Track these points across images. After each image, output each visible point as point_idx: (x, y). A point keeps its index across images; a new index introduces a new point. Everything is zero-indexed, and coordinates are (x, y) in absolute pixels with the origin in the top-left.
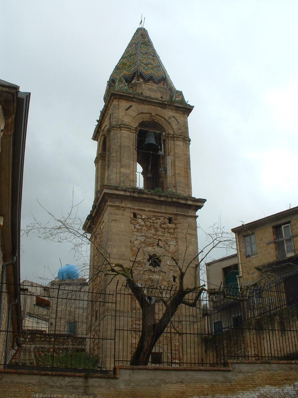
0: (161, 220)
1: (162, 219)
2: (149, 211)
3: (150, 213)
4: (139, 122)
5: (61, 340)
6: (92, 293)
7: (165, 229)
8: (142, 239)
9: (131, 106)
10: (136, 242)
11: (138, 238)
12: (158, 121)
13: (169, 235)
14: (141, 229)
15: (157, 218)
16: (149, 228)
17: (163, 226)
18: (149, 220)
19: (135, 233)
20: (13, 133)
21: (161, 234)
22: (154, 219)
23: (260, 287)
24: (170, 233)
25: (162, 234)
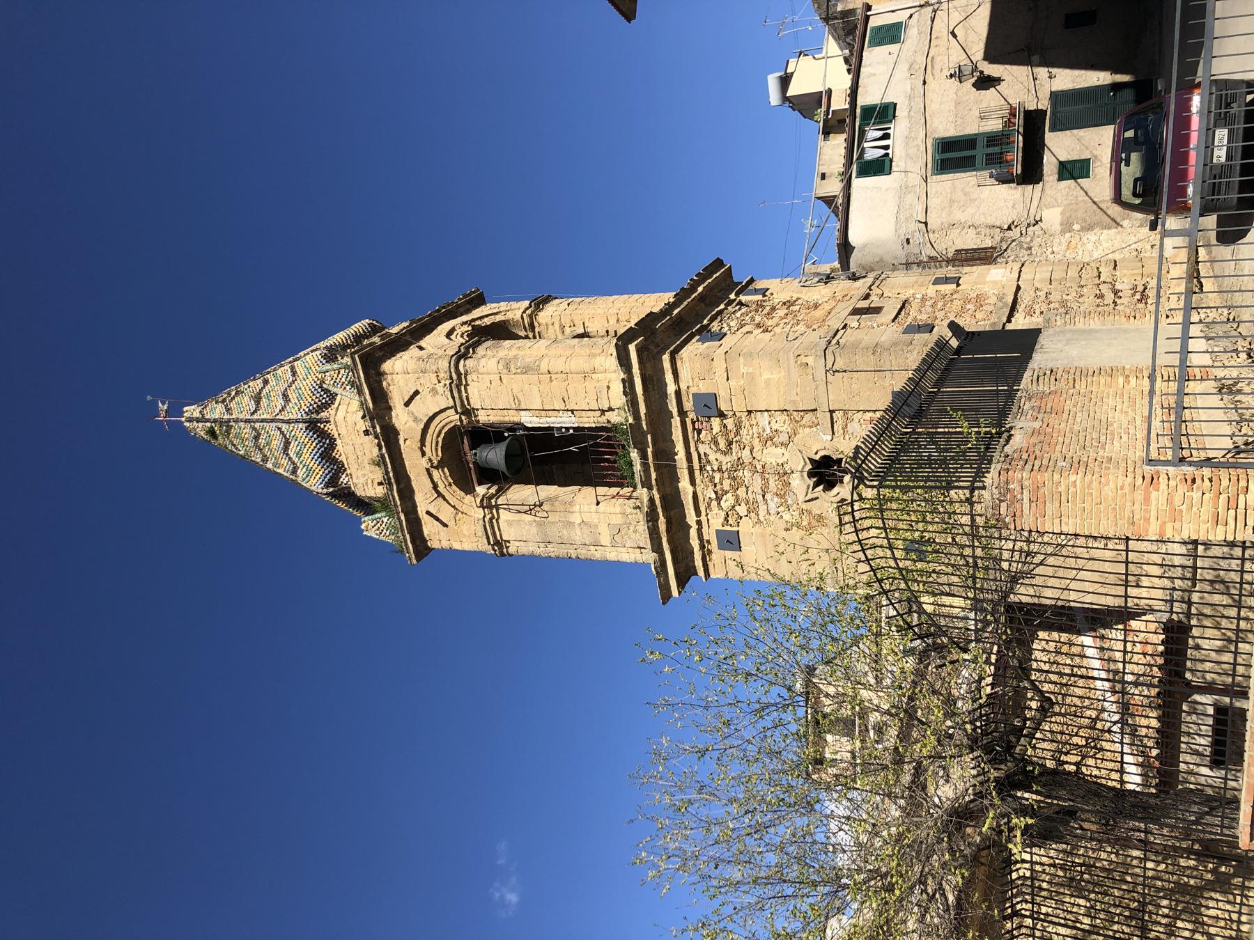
0: (709, 451)
1: (703, 448)
2: (693, 482)
3: (698, 481)
4: (463, 494)
5: (978, 724)
6: (1127, 563)
7: (730, 443)
8: (773, 502)
9: (428, 513)
10: (787, 516)
11: (772, 512)
12: (440, 432)
13: (744, 432)
14: (747, 502)
15: (704, 462)
16: (737, 483)
17: (722, 445)
18: (717, 480)
19: (762, 519)
20: (1214, 682)
21: (747, 452)
22: (708, 468)
23: (965, 181)
24: (739, 425)
25: (747, 448)
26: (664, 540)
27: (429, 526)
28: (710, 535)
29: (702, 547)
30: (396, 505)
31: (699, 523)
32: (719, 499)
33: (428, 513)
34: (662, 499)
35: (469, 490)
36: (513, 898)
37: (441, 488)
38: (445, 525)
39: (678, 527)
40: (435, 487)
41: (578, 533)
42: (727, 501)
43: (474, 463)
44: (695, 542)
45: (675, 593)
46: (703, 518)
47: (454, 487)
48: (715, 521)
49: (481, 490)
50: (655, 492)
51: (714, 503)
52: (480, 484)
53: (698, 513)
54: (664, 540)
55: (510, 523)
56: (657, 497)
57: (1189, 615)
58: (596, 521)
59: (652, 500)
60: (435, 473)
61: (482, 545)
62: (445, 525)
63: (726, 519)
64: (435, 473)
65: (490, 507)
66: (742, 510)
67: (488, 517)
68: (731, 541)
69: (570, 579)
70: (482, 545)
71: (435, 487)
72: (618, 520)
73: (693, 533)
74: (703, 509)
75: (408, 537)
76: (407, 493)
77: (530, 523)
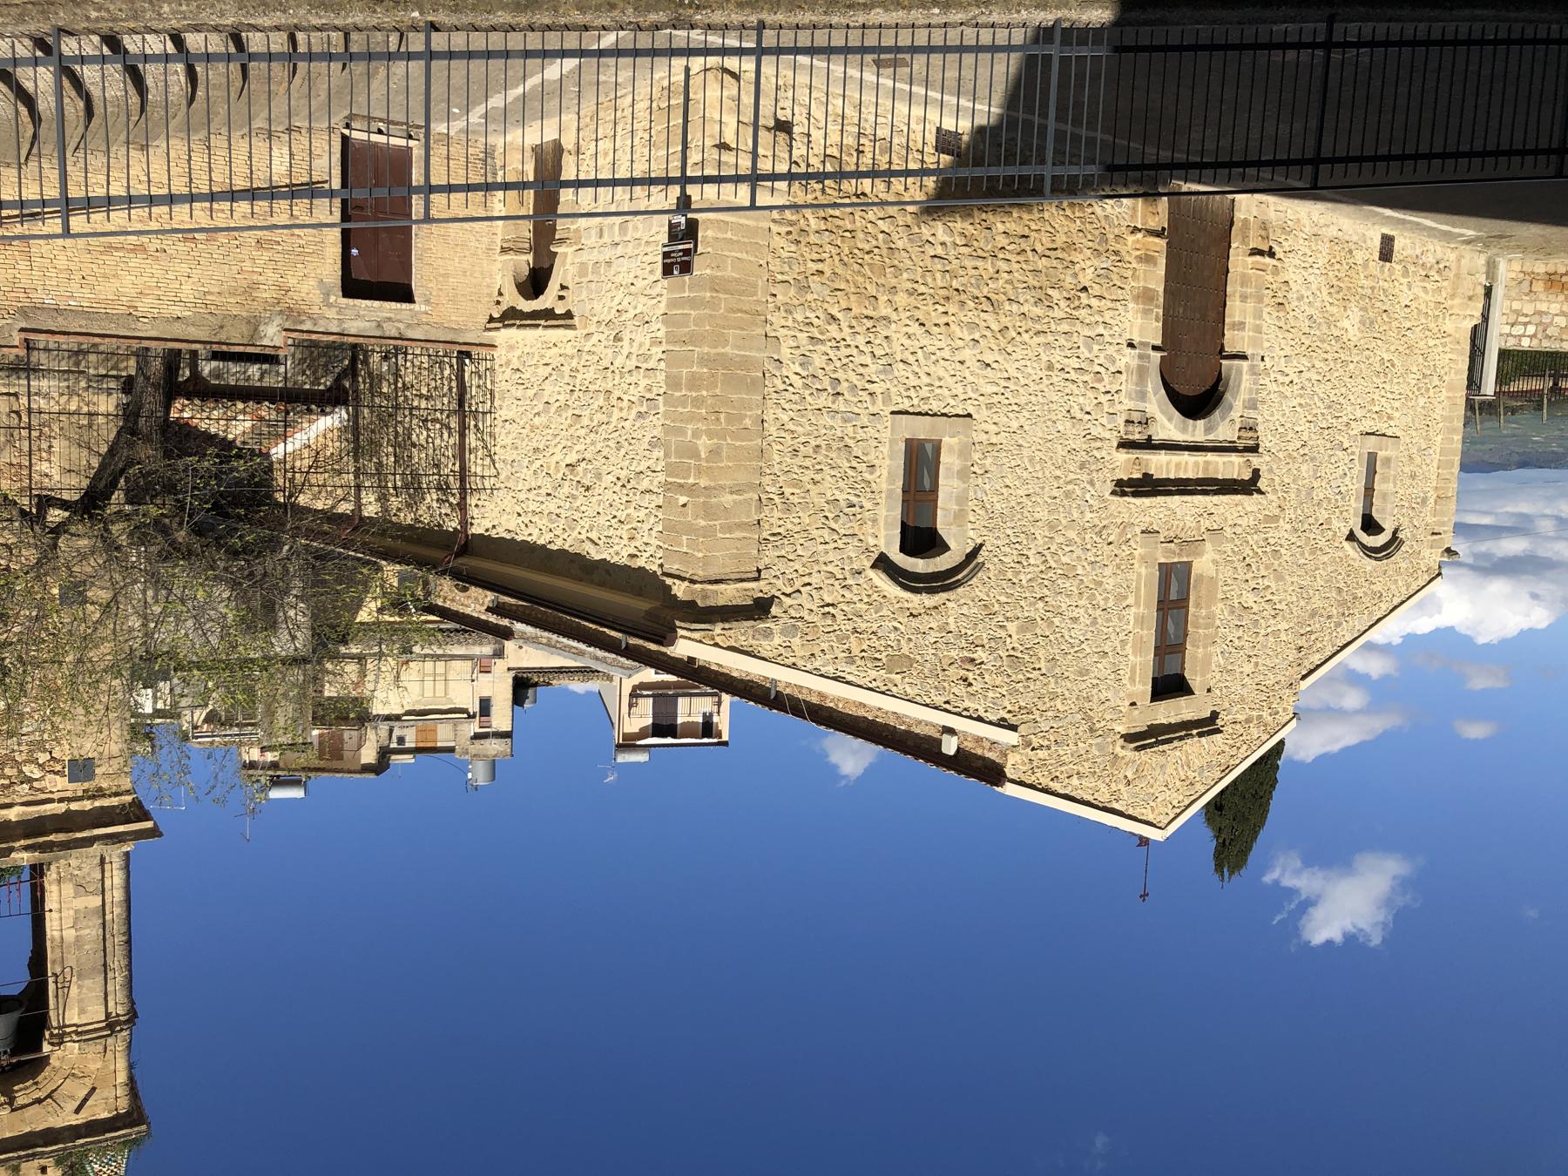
9: (77, 1111)
26: (79, 835)
27: (97, 1110)
28: (79, 788)
29: (93, 797)
30: (64, 1149)
31: (61, 800)
32: (30, 780)
33: (77, 1111)
34: (27, 837)
35: (45, 1061)
36: (1100, 1141)
37: (42, 1095)
38: (94, 1089)
39: (67, 822)
40: (39, 1101)
41: (87, 931)
42: (31, 771)
43: (13, 1055)
44: (87, 805)
45: (149, 824)
46: (56, 796)
47: (39, 1079)
48: (59, 784)
49: (46, 1048)
50: (17, 845)
51: (36, 784)
52: (39, 1049)
53: (51, 801)
54: (79, 835)
55: (82, 1011)
56: (22, 842)
57: (117, 377)
58: (72, 912)
59: (26, 848)
60: (20, 1101)
61: (118, 1043)
62: (94, 1089)
63: (56, 773)
64: (20, 1101)
65: (61, 1036)
66: (43, 758)
67: (75, 1037)
68: (81, 769)
69: (132, 933)
70: (118, 1043)
71: (39, 1101)
72: (68, 889)
73: (74, 806)
74: (44, 796)
75: (108, 1135)
76: (50, 1136)
77: (80, 987)
